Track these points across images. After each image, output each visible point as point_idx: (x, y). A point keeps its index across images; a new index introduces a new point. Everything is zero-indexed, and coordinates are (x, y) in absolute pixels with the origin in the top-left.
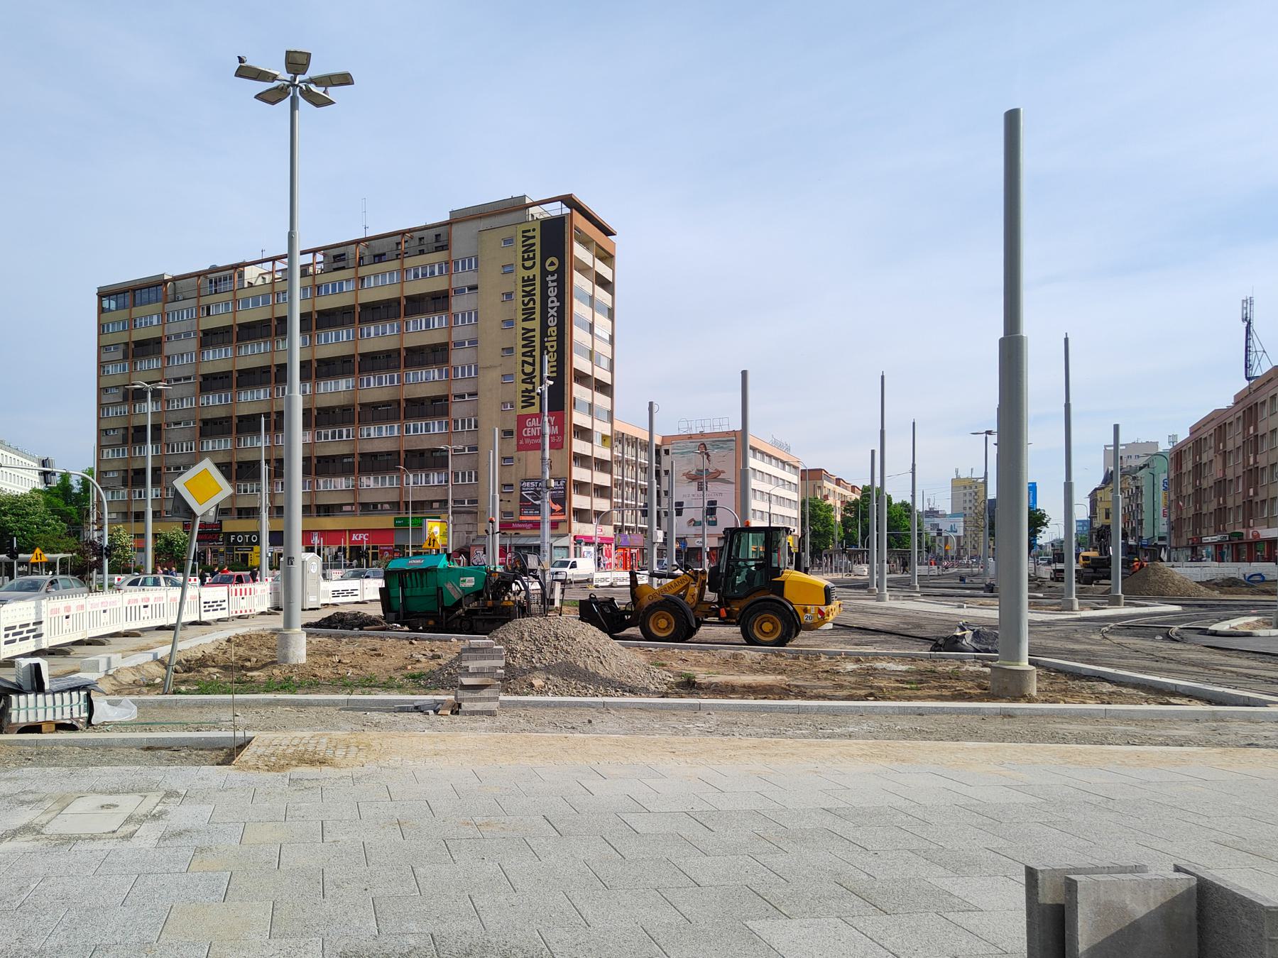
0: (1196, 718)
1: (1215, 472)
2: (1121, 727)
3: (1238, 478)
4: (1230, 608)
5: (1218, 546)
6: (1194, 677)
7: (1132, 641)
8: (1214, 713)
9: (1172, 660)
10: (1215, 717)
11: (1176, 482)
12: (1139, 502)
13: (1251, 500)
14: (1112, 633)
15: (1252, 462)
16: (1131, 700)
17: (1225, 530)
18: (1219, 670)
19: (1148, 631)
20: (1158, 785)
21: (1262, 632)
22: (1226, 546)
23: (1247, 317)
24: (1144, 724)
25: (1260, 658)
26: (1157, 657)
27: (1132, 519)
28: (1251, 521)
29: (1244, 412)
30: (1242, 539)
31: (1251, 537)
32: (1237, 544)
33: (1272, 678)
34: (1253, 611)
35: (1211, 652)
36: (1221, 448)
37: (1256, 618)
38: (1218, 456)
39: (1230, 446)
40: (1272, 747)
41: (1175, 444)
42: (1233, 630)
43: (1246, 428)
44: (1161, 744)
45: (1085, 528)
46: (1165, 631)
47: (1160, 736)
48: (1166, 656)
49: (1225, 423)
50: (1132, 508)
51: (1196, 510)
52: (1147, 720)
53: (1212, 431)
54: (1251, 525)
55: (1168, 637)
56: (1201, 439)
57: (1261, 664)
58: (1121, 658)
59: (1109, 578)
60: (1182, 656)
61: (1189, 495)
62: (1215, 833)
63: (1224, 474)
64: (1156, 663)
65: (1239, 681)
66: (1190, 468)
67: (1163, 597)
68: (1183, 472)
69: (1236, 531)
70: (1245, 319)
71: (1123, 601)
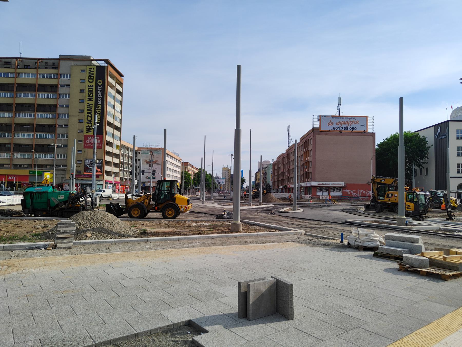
1: (281, 170)
3: (286, 171)
5: (282, 189)
7: (264, 215)
10: (281, 235)
11: (273, 172)
18: (282, 222)
21: (290, 212)
36: (289, 160)
37: (289, 208)
43: (288, 159)
44: (270, 243)
47: (269, 240)
55: (271, 213)
66: (277, 168)
67: (270, 202)
70: (288, 131)
71: (262, 203)
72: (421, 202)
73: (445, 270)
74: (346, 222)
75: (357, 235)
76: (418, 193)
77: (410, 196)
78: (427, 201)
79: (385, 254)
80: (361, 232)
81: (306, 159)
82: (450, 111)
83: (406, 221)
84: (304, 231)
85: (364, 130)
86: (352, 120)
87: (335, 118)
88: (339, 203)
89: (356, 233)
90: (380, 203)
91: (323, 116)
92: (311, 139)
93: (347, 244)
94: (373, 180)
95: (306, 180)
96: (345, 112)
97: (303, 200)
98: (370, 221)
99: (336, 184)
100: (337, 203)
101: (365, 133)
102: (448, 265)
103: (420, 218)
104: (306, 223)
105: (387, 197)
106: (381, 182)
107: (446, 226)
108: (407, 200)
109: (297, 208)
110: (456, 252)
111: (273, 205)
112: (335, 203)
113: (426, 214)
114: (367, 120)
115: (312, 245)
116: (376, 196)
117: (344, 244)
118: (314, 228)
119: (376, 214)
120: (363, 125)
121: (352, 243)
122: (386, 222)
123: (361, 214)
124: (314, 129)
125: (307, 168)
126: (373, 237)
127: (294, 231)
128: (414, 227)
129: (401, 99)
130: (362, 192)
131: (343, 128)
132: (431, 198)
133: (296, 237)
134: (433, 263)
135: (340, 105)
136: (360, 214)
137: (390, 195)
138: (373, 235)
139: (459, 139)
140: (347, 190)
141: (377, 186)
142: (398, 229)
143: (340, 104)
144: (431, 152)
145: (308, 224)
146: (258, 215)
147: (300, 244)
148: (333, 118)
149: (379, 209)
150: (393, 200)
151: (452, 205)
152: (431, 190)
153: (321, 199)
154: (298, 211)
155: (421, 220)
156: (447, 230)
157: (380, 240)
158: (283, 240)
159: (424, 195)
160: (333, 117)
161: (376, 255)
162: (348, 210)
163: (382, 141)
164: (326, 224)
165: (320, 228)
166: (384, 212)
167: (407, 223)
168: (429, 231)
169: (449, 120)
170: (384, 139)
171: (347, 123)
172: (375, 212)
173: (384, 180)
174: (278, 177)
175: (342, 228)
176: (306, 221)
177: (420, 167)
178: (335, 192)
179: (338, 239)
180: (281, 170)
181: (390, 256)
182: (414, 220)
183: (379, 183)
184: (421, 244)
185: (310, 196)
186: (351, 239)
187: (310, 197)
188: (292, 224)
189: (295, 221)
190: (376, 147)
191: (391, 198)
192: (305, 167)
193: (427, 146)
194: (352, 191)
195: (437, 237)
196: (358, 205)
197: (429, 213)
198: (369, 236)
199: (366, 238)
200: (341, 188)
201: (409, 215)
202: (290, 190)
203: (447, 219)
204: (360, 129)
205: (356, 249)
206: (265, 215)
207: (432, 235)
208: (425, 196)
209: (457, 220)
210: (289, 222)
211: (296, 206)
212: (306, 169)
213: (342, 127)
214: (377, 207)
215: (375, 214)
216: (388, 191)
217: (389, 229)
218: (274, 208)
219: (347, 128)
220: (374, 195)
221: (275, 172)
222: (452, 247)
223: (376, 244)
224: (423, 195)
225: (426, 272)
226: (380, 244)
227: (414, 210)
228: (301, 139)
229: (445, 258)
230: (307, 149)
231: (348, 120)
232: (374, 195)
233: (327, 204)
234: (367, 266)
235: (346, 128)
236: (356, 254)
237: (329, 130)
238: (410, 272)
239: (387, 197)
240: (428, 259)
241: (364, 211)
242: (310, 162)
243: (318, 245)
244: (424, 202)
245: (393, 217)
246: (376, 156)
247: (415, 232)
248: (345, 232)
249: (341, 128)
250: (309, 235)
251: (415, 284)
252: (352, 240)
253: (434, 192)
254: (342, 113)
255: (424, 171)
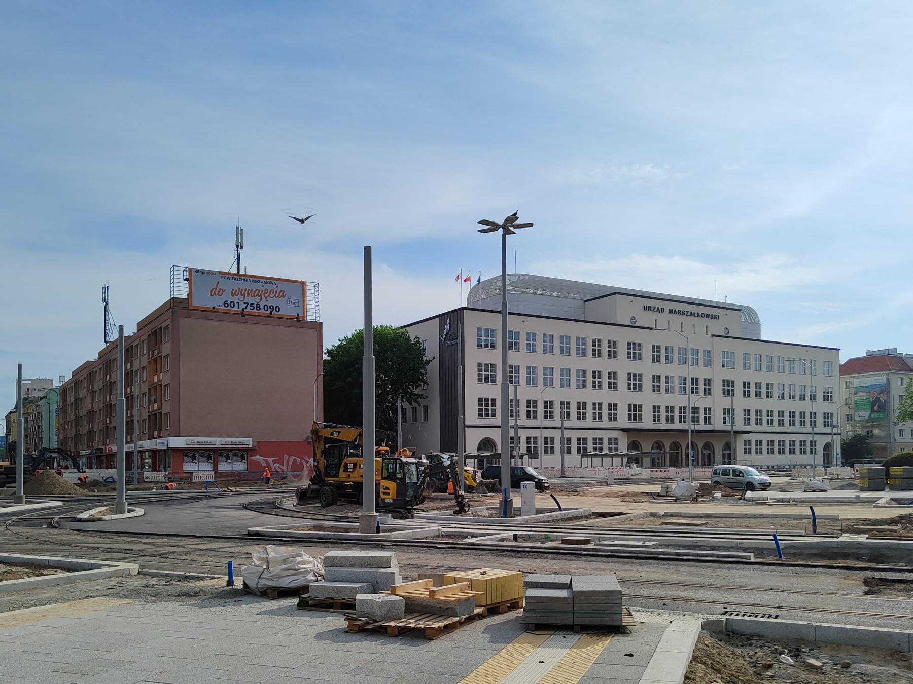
0: (57, 583)
1: (86, 406)
2: (7, 598)
3: (100, 410)
4: (92, 501)
5: (89, 457)
6: (61, 553)
7: (25, 531)
8: (69, 577)
9: (50, 542)
10: (69, 580)
11: (63, 411)
12: (40, 424)
13: (108, 426)
14: (13, 525)
15: (108, 400)
16: (17, 576)
17: (93, 446)
18: (78, 546)
19: (39, 521)
20: (23, 638)
21: (107, 517)
22: (93, 458)
23: (105, 300)
24: (23, 593)
25: (104, 535)
26: (40, 540)
27: (35, 437)
28: (108, 440)
29: (104, 365)
30: (103, 453)
31: (107, 452)
32: (100, 457)
33: (108, 548)
34: (105, 503)
35: (75, 534)
36: (108, 379)
37: (105, 508)
38: (89, 394)
39: (96, 388)
40: (99, 596)
41: (64, 382)
42: (91, 517)
43: (105, 377)
44: (32, 606)
45: (3, 443)
46: (49, 520)
47: (32, 600)
48: (47, 540)
49: (133, 345)
50: (35, 429)
51: (76, 432)
52: (25, 590)
53: (85, 376)
54: (108, 443)
55: (51, 526)
56: (110, 360)
57: (103, 539)
58: (16, 544)
59: (15, 482)
60: (57, 538)
61: (72, 421)
62: (54, 664)
63: (92, 408)
64: (38, 545)
65: (88, 553)
66: (72, 401)
67: (52, 495)
68: (68, 404)
69: (100, 447)
70: (104, 301)
71: (24, 500)
72: (410, 478)
73: (432, 619)
74: (249, 534)
75: (262, 564)
76: (404, 459)
77: (389, 467)
78: (421, 477)
79: (322, 600)
80: (272, 554)
81: (156, 380)
82: (467, 288)
83: (378, 522)
84: (137, 566)
85: (298, 315)
86: (269, 287)
87: (229, 278)
88: (237, 490)
89: (260, 559)
90: (330, 485)
91: (197, 271)
92: (166, 328)
93: (242, 587)
94: (315, 432)
95: (156, 434)
96: (254, 265)
97: (147, 486)
98: (303, 528)
99: (198, 442)
100: (233, 489)
101: (299, 321)
102: (438, 607)
103: (407, 514)
104: (146, 543)
105: (344, 472)
106: (332, 437)
107: (452, 528)
108: (384, 476)
109: (127, 507)
110: (455, 577)
111: (60, 503)
112: (228, 489)
113: (418, 504)
114: (303, 290)
115: (154, 598)
116: (322, 470)
117: (236, 587)
118: (164, 556)
119: (322, 511)
120: (295, 303)
121: (252, 584)
122: (339, 526)
123: (286, 513)
124: (173, 300)
125: (158, 400)
126: (299, 563)
127: (110, 566)
128: (392, 533)
129: (368, 250)
130: (295, 460)
131: (248, 304)
132: (428, 470)
133: (114, 583)
134: (412, 607)
135: (240, 247)
136: (285, 513)
137: (350, 466)
138: (299, 559)
139: (482, 347)
140: (258, 457)
141: (324, 446)
142: (361, 540)
143: (239, 246)
144: (433, 371)
145: (150, 546)
146: (9, 532)
147: (121, 601)
148: (222, 277)
149: (328, 499)
150: (355, 477)
151: (467, 482)
152: (431, 453)
153: (194, 481)
154: (130, 515)
155: (409, 518)
156: (453, 535)
157: (316, 570)
158: (74, 594)
159: (416, 463)
160: (224, 276)
161: (303, 605)
162: (257, 505)
163: (337, 343)
164: (197, 544)
165: (180, 554)
166: (338, 504)
167: (380, 527)
168: (421, 539)
169: (466, 306)
170: (339, 340)
171: (258, 294)
172: (320, 505)
173: (339, 432)
174: (77, 425)
175: (236, 550)
176: (147, 538)
177: (413, 403)
178: (196, 461)
179: (222, 576)
180: (86, 406)
181: (332, 603)
182: (395, 517)
183: (327, 440)
184: (394, 569)
185: (167, 473)
186: (250, 573)
187: (165, 477)
188: (109, 550)
189: (117, 542)
190: (325, 357)
191: (352, 472)
192: (153, 398)
193: (424, 359)
194: (270, 460)
195: (433, 550)
196: (283, 492)
197: (426, 502)
198: (291, 562)
199: (283, 567)
200: (243, 453)
201: (387, 508)
202: (105, 460)
203: (456, 513)
204: (287, 310)
205: (261, 596)
206: (29, 530)
207: (424, 548)
208: (417, 465)
209: (472, 513)
210: (99, 545)
211: (124, 501)
212: (156, 406)
213: (245, 302)
214: (324, 494)
215: (319, 511)
216: (346, 457)
217: (343, 543)
218: (58, 511)
219: (257, 305)
220: (317, 466)
221: (69, 412)
222: (456, 568)
223: (307, 578)
224: (413, 463)
225: (398, 628)
226: (314, 578)
227: (397, 497)
228: (142, 325)
229: (432, 593)
230: (156, 351)
231: (259, 286)
232: (317, 466)
233: (208, 492)
234: (280, 632)
235: (255, 307)
236: (260, 607)
237: (214, 308)
238: (368, 633)
239: (344, 472)
240: (402, 599)
241: (295, 504)
242: (165, 386)
243: (170, 596)
244: (415, 480)
245: (356, 515)
246: (324, 375)
247: (393, 545)
248: (241, 559)
249: (242, 306)
250: (151, 574)
251: (373, 656)
252: (252, 575)
253: (437, 458)
254: (245, 267)
255: (421, 411)
